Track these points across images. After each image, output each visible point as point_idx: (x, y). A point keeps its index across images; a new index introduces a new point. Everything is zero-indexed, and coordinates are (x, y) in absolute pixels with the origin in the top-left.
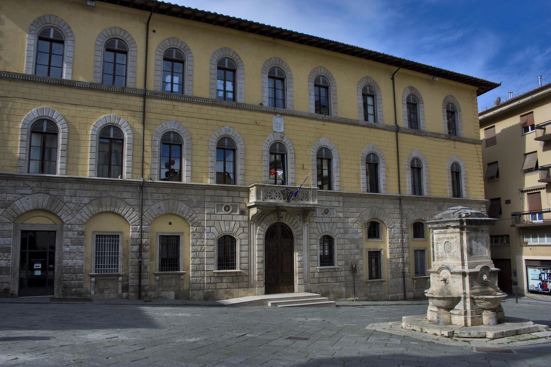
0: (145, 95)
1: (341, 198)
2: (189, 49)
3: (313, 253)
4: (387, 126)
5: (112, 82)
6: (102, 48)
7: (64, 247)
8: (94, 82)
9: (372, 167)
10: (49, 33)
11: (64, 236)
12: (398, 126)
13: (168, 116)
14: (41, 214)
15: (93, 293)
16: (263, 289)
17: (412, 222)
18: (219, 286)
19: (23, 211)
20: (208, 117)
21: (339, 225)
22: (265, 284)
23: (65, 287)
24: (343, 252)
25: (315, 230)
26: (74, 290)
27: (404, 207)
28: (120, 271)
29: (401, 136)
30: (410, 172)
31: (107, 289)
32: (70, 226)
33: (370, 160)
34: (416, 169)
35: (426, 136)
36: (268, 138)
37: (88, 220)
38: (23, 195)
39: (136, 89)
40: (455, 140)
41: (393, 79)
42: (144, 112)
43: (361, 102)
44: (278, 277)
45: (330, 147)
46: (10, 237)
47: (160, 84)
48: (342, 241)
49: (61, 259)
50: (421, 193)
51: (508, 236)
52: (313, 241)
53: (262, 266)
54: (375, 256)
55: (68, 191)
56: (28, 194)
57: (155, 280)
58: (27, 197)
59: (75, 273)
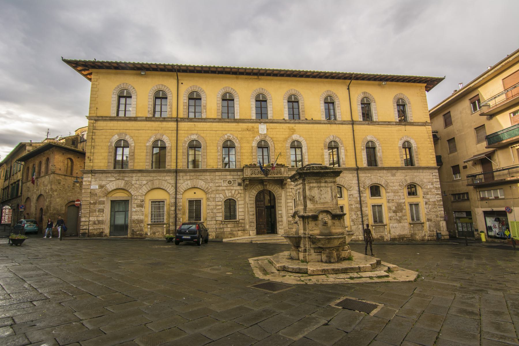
0: (177, 120)
12: (353, 121)
13: (189, 131)
14: (121, 191)
19: (111, 190)
25: (291, 194)
26: (138, 233)
40: (405, 125)
41: (348, 89)
42: (177, 130)
43: (152, 103)
45: (374, 140)
47: (186, 113)
51: (467, 193)
52: (289, 201)
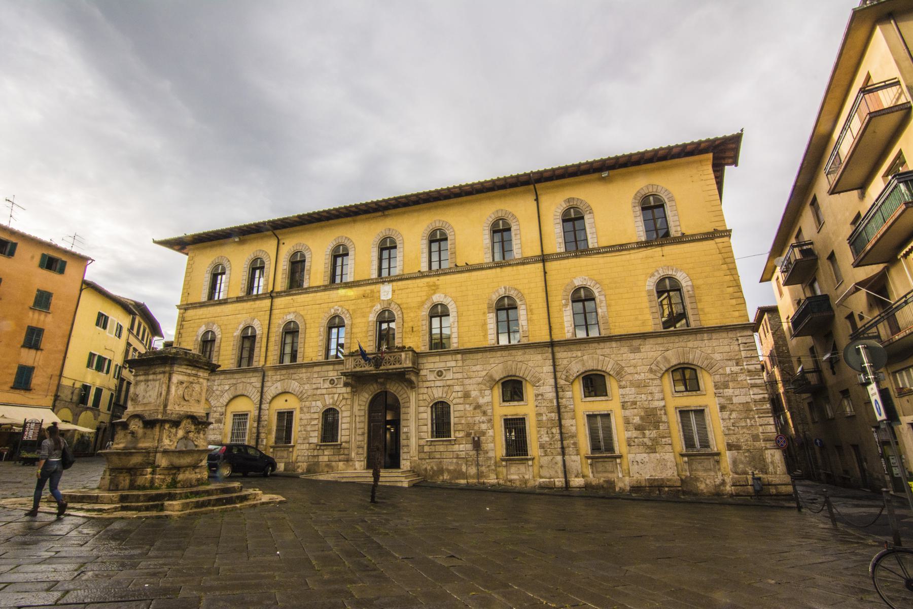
1: (459, 357)
3: (421, 422)
6: (638, 209)
21: (457, 388)
52: (422, 409)
54: (515, 426)
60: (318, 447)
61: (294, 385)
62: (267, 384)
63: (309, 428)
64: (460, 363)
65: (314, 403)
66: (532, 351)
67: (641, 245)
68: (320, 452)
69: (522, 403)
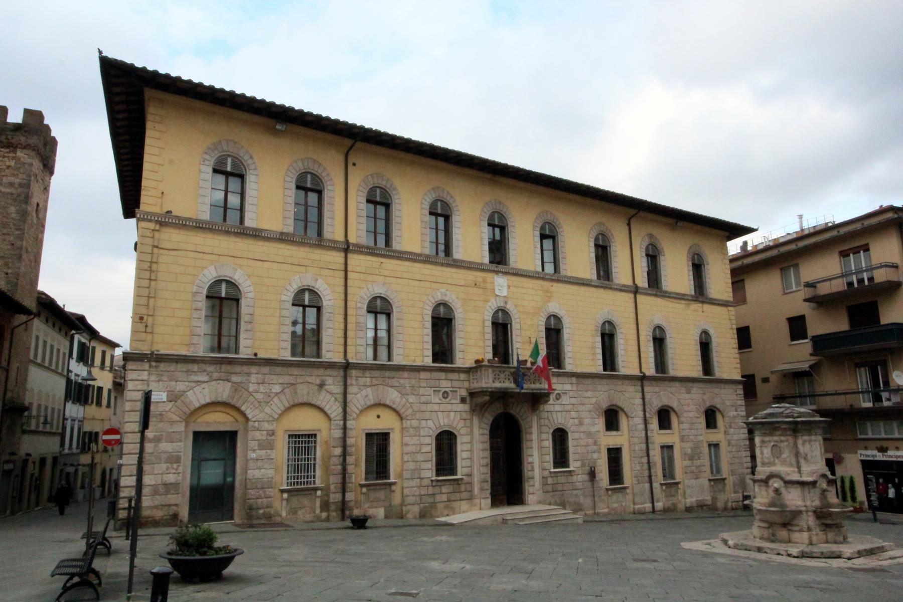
0: (347, 248)
1: (574, 380)
2: (395, 189)
4: (624, 286)
5: (309, 229)
7: (249, 452)
8: (285, 231)
9: (608, 338)
10: (226, 164)
11: (250, 438)
15: (284, 514)
16: (489, 501)
17: (656, 409)
18: (438, 498)
19: (197, 405)
20: (418, 277)
21: (574, 414)
22: (491, 494)
23: (251, 508)
24: (579, 450)
26: (261, 511)
27: (646, 389)
28: (318, 483)
29: (640, 298)
30: (651, 344)
31: (300, 508)
32: (256, 424)
33: (498, 317)
34: (659, 341)
35: (669, 297)
36: (490, 304)
37: (281, 415)
38: (199, 382)
39: (335, 242)
40: (703, 302)
44: (508, 485)
46: (180, 441)
48: (576, 436)
49: (246, 470)
50: (613, 368)
52: (544, 436)
53: (488, 470)
54: (614, 455)
55: (254, 376)
56: (204, 382)
57: (362, 493)
58: (203, 386)
59: (263, 488)
60: (434, 484)
61: (392, 396)
62: (351, 390)
63: (420, 457)
64: (575, 389)
65: (424, 422)
66: (627, 382)
67: (282, 238)
68: (437, 490)
69: (619, 433)
